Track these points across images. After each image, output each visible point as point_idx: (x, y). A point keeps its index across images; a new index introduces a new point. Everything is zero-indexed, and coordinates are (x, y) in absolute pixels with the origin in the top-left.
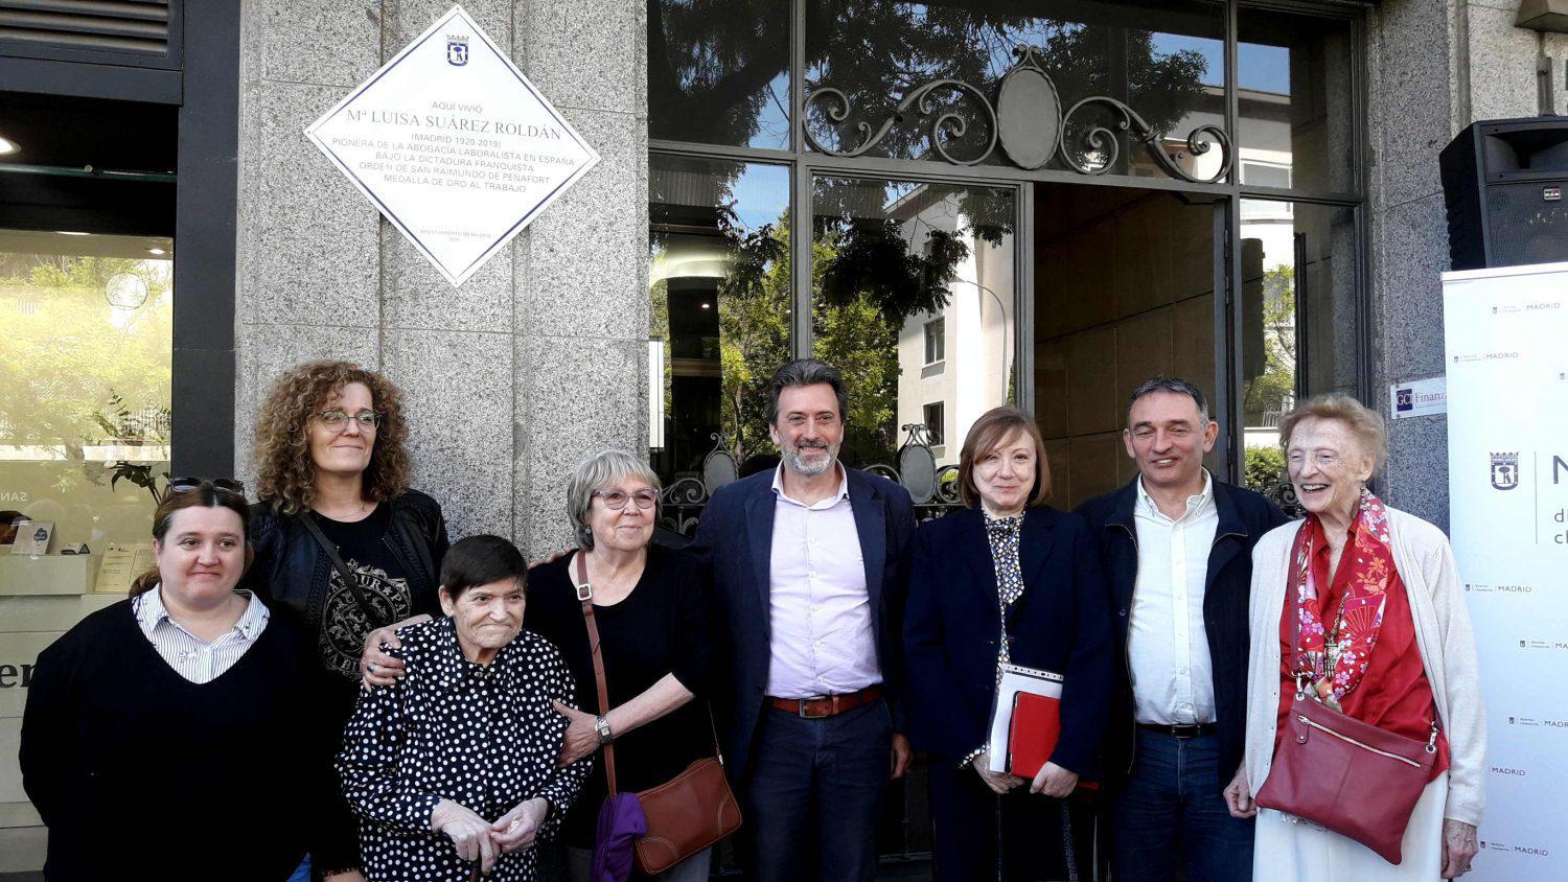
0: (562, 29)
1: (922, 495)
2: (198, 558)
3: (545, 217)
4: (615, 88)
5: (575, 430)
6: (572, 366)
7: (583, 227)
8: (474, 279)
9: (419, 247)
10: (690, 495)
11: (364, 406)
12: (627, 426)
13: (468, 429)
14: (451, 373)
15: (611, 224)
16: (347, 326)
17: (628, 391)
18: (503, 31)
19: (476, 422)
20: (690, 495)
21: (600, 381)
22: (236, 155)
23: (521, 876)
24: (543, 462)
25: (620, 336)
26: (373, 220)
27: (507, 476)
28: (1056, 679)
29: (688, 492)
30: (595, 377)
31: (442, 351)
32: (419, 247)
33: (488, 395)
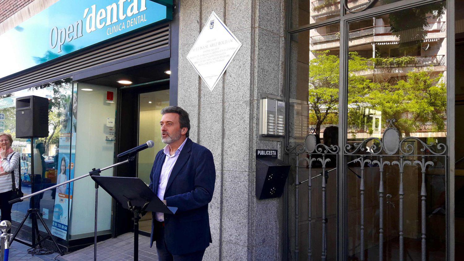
0: (234, 8)
1: (392, 151)
2: (95, 173)
3: (229, 66)
4: (246, 21)
5: (235, 130)
6: (234, 110)
7: (238, 67)
8: (215, 89)
9: (205, 83)
10: (348, 146)
11: (169, 120)
12: (246, 128)
13: (213, 131)
14: (210, 116)
15: (244, 64)
16: (193, 106)
17: (247, 117)
18: (222, 14)
19: (215, 128)
20: (348, 146)
21: (240, 114)
22: (178, 67)
23: (271, 191)
24: (228, 140)
25: (245, 100)
26: (198, 76)
27: (220, 144)
28: (282, 123)
29: (350, 146)
30: (239, 113)
31: (209, 110)
32: (205, 83)
33: (217, 121)
